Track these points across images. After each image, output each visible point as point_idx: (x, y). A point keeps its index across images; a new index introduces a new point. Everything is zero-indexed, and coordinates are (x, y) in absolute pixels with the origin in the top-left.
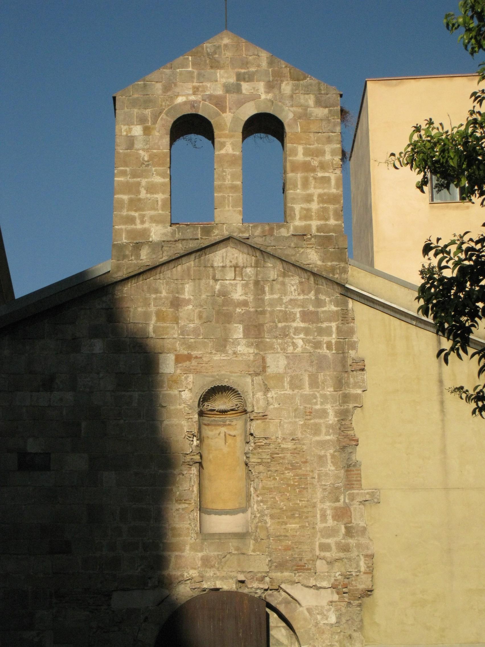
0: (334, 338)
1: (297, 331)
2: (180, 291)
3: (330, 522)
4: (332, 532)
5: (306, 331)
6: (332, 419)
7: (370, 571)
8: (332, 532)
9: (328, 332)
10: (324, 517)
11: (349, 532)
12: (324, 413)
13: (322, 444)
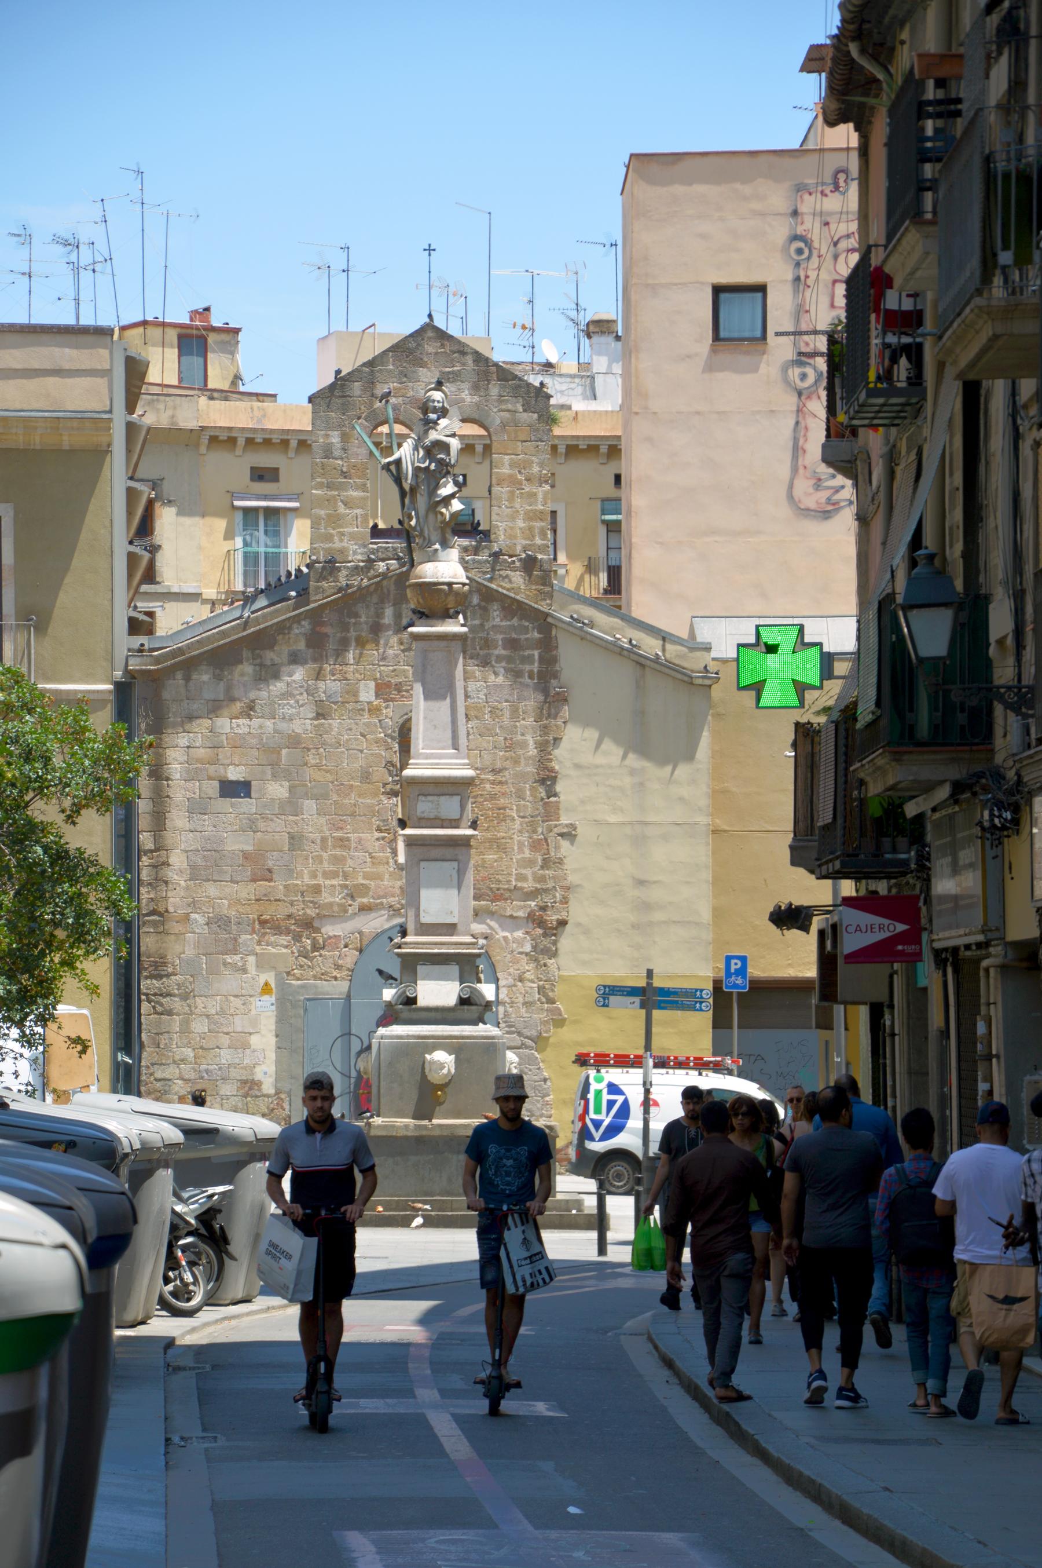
0: (535, 667)
1: (499, 659)
2: (379, 615)
3: (527, 853)
4: (531, 863)
5: (509, 660)
6: (532, 751)
7: (565, 901)
8: (531, 863)
9: (529, 659)
10: (521, 850)
11: (546, 864)
12: (524, 745)
13: (523, 776)
